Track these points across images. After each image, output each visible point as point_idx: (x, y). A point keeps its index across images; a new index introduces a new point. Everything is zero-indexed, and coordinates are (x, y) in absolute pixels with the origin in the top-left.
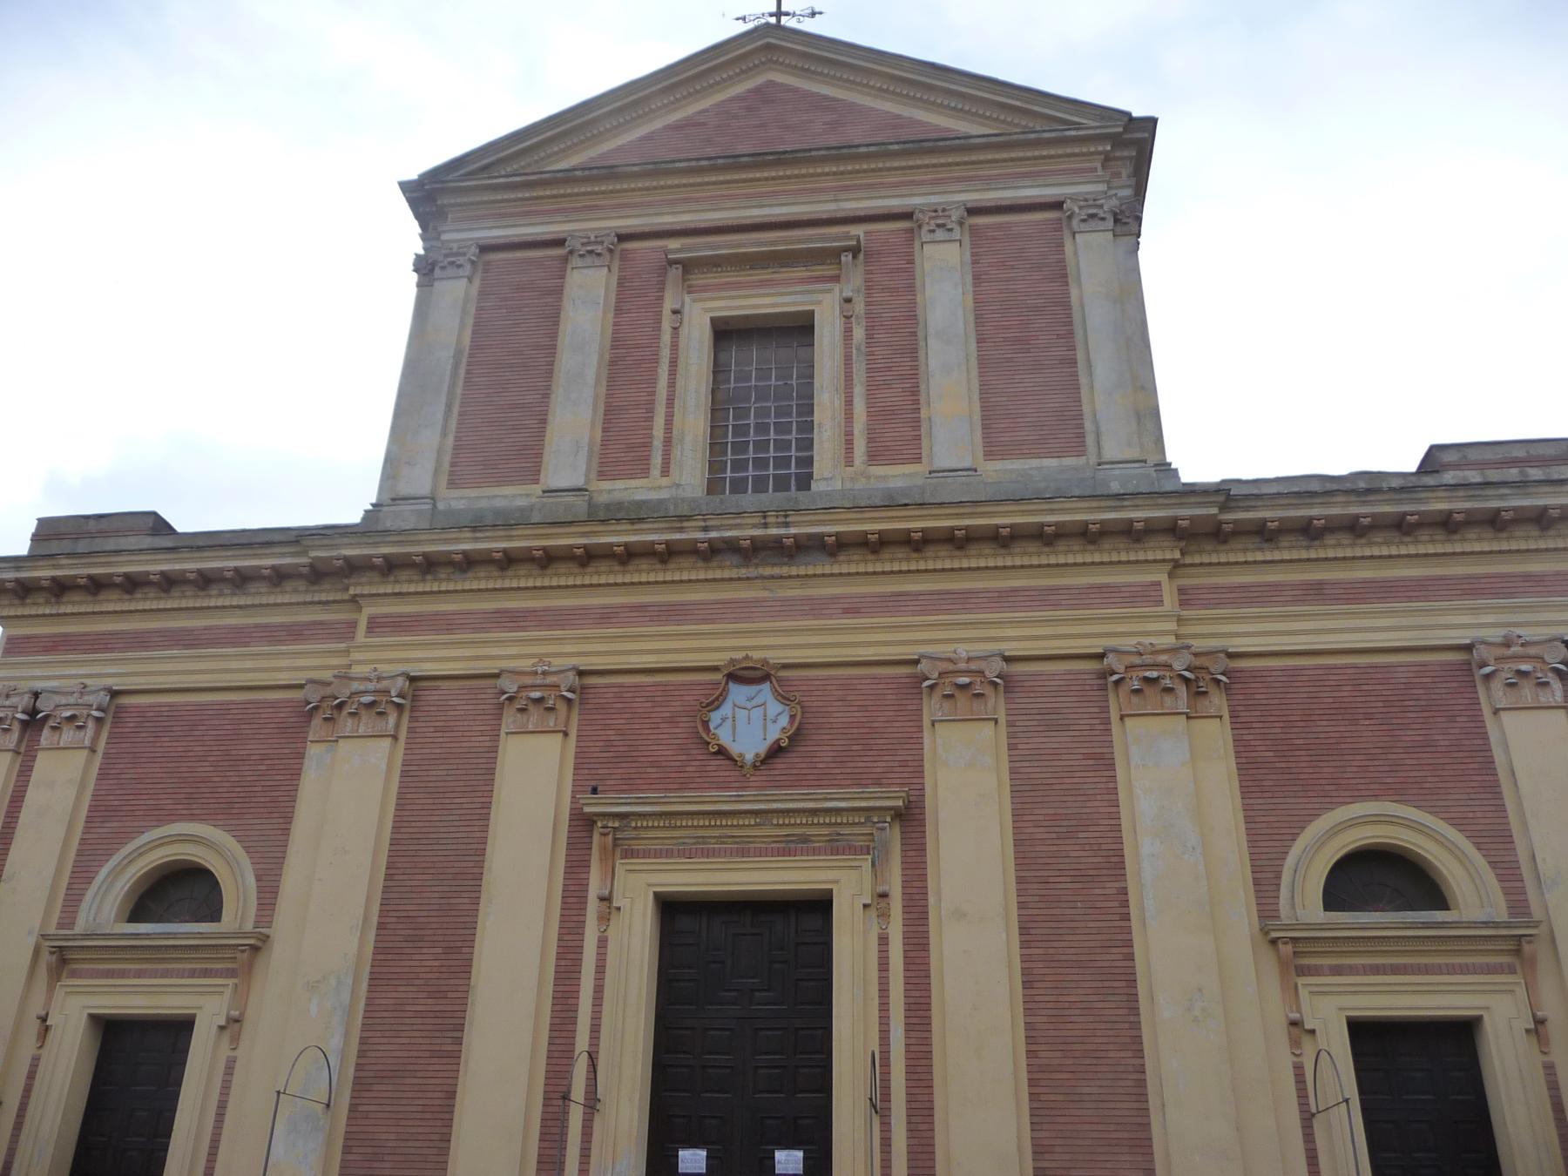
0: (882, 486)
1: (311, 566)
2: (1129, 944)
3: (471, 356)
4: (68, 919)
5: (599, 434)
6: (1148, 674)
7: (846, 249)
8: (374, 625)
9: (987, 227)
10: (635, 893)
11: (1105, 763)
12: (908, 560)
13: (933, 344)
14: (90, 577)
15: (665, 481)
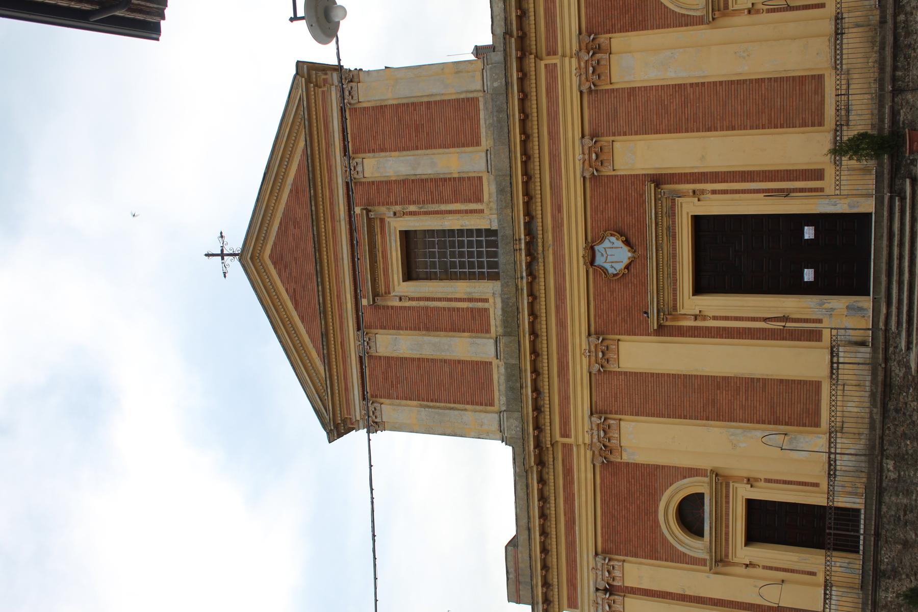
0: (494, 195)
1: (537, 465)
2: (715, 83)
4: (702, 562)
5: (466, 334)
6: (591, 72)
8: (565, 434)
10: (692, 304)
11: (632, 92)
12: (535, 182)
13: (419, 172)
14: (542, 569)
15: (491, 301)
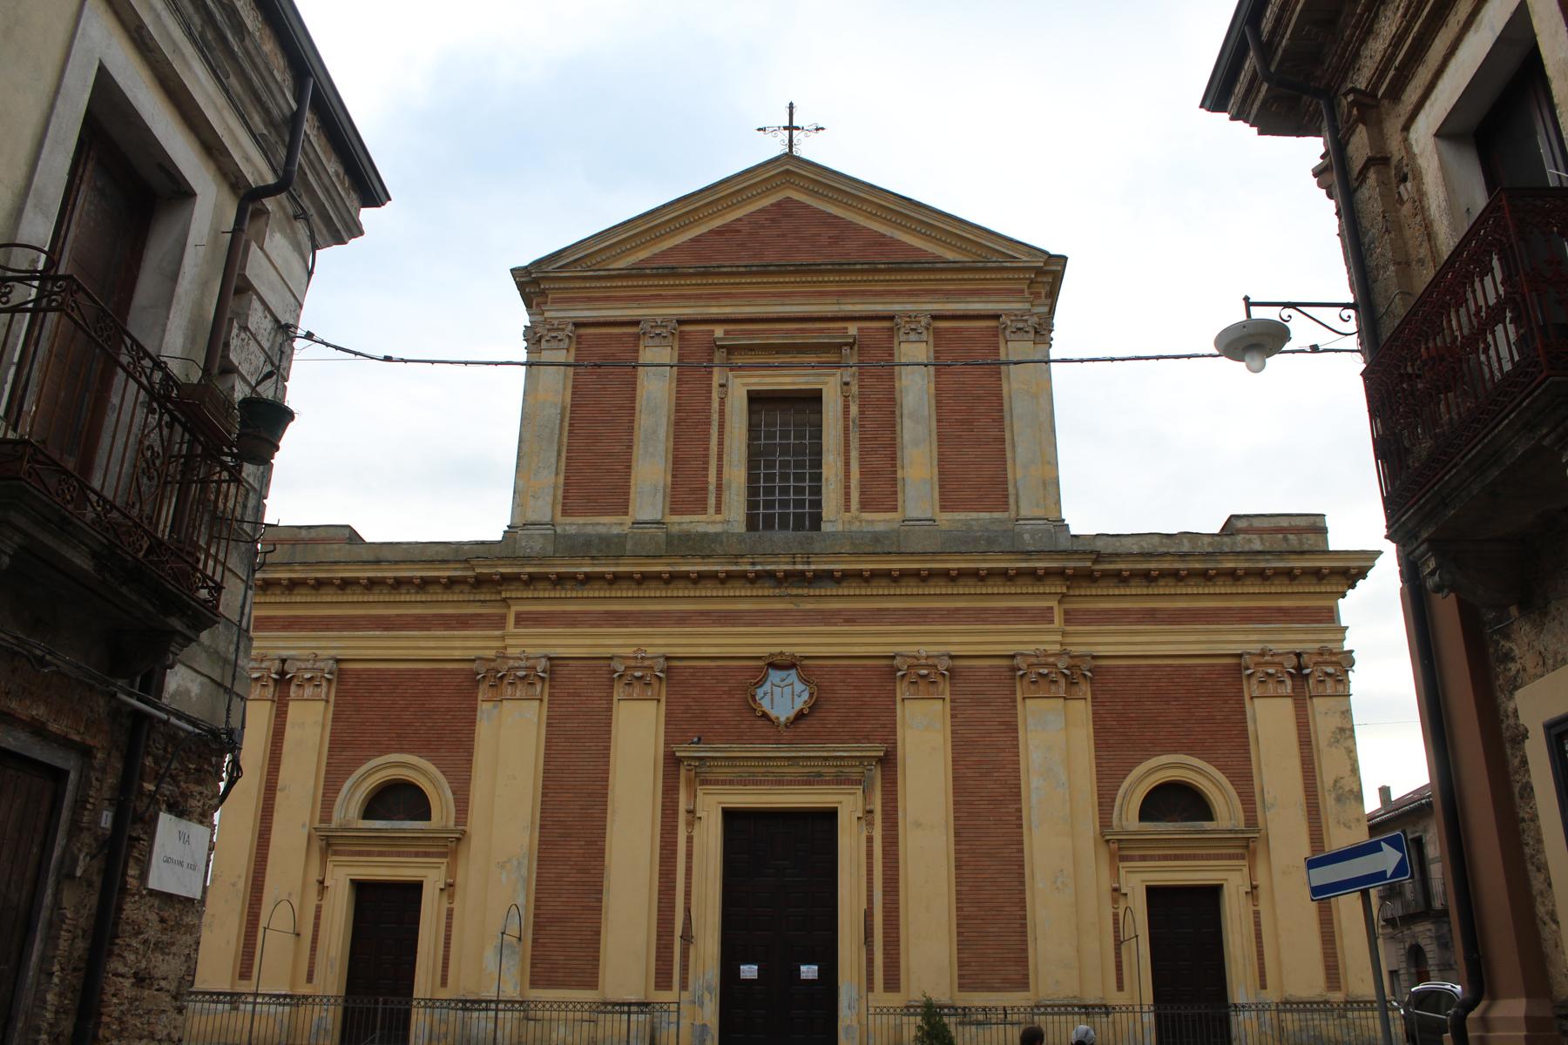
0: (870, 529)
2: (1021, 843)
3: (572, 412)
5: (669, 479)
7: (846, 344)
8: (520, 620)
9: (947, 330)
10: (711, 806)
13: (907, 422)
15: (718, 518)
